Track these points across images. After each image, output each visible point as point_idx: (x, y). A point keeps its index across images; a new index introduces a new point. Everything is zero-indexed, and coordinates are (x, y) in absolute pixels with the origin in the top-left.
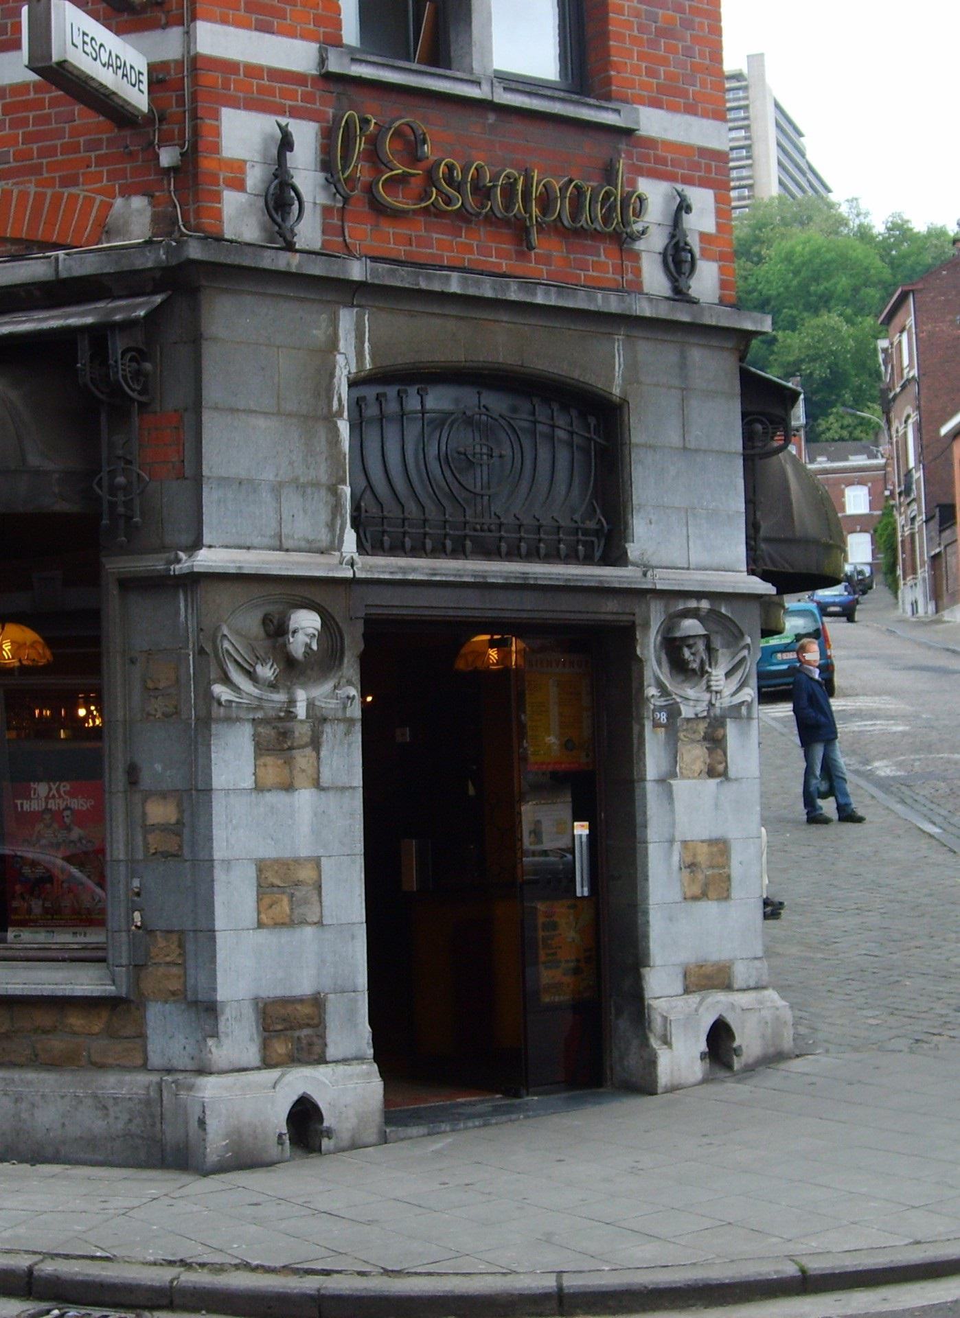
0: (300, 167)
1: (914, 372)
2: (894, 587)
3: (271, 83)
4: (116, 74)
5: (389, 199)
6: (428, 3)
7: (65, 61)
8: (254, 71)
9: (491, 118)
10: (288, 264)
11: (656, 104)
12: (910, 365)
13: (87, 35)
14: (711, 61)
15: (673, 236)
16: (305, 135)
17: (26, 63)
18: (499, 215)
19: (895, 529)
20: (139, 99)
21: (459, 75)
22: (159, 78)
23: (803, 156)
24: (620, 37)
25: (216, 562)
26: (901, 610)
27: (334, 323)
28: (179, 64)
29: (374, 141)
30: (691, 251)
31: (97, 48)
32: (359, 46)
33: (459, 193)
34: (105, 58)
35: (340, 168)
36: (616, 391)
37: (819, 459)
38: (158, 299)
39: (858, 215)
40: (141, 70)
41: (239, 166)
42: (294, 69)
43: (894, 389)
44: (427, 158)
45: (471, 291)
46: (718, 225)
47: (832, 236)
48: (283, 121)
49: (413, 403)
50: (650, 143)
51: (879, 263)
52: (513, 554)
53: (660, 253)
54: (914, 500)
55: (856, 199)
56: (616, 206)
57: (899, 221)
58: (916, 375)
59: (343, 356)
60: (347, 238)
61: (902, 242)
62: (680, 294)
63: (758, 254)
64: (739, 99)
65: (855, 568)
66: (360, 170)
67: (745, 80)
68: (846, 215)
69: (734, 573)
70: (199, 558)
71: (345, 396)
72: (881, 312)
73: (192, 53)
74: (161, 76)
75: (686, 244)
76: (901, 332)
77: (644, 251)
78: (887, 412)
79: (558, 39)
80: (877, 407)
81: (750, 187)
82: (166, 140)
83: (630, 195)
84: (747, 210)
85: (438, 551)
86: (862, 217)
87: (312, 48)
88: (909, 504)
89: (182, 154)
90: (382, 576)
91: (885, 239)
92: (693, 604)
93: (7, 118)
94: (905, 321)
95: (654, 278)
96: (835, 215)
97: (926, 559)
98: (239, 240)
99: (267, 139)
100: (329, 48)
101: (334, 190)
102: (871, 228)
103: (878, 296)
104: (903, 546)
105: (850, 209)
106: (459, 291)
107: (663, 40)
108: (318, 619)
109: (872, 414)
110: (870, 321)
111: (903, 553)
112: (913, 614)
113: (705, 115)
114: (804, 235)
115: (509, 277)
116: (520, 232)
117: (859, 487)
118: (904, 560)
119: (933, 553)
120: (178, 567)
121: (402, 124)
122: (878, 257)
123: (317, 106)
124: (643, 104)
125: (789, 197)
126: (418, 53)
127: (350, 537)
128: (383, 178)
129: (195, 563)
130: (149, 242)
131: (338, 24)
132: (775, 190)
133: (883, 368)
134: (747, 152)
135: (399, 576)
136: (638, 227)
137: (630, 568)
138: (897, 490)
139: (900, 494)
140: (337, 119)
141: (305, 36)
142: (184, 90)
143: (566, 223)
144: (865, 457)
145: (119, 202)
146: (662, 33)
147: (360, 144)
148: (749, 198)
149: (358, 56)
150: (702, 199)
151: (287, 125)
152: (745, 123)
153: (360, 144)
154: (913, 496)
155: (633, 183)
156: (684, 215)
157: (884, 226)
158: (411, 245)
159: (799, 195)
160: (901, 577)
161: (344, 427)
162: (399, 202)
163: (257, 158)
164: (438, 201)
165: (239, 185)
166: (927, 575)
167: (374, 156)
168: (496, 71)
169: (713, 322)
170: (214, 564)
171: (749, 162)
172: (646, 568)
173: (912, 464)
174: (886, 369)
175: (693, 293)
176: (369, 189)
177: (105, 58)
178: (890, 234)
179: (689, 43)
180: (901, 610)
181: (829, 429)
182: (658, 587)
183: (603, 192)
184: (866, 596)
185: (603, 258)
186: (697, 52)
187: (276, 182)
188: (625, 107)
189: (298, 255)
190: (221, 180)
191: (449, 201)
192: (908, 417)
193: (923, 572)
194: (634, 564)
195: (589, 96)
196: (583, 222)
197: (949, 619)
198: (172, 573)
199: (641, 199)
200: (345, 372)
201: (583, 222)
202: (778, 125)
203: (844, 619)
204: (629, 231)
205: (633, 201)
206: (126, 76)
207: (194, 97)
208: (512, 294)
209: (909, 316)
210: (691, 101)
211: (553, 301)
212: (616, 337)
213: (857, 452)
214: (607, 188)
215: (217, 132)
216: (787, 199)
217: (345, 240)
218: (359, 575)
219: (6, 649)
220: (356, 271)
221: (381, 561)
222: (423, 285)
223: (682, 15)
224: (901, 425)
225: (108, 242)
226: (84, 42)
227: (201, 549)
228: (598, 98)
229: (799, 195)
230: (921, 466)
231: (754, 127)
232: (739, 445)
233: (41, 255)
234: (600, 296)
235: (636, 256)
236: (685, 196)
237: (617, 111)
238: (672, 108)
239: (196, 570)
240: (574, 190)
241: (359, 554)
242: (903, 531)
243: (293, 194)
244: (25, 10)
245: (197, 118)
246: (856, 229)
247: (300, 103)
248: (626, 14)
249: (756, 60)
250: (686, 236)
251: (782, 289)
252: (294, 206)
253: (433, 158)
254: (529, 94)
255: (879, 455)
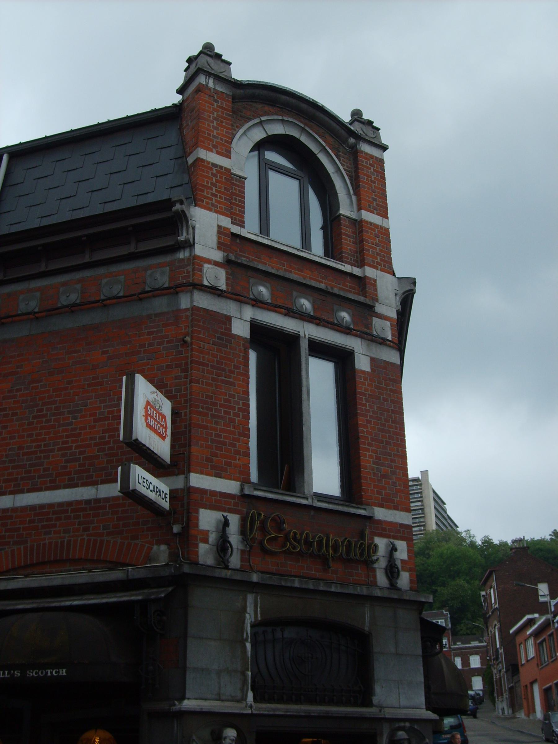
0: (232, 533)
1: (497, 606)
2: (494, 702)
3: (220, 499)
4: (156, 495)
5: (268, 547)
6: (286, 465)
7: (135, 490)
8: (214, 493)
9: (312, 513)
10: (226, 575)
11: (381, 506)
12: (495, 603)
13: (145, 479)
14: (404, 488)
15: (389, 561)
16: (234, 520)
17: (119, 490)
18: (316, 553)
19: (492, 675)
20: (165, 504)
21: (299, 495)
22: (174, 495)
23: (446, 512)
24: (366, 467)
25: (191, 706)
26: (497, 713)
27: (245, 600)
28: (182, 490)
29: (263, 523)
30: (397, 568)
31: (149, 484)
32: (257, 483)
33: (299, 544)
34: (152, 488)
35: (248, 534)
36: (367, 629)
37: (458, 643)
38: (170, 589)
39: (470, 537)
40: (167, 493)
41: (206, 533)
42: (230, 492)
43: (489, 613)
44: (285, 530)
45: (304, 586)
46: (409, 556)
47: (459, 547)
48: (225, 514)
49: (279, 635)
50: (379, 522)
51: (479, 557)
52: (322, 702)
53: (384, 569)
54: (500, 662)
55: (469, 530)
56: (365, 549)
57: (487, 540)
58: (498, 607)
59: (248, 614)
60: (251, 564)
61: (489, 549)
62: (393, 586)
63: (428, 554)
64: (418, 489)
65: (476, 692)
66: (257, 534)
67: (420, 481)
68: (465, 537)
69: (420, 710)
70: (184, 704)
71: (249, 632)
72: (482, 579)
73: (188, 486)
74: (175, 495)
75: (395, 565)
76: (491, 588)
77: (377, 568)
78: (486, 623)
79: (340, 479)
80: (482, 620)
81: (424, 526)
82: (176, 522)
83: (371, 544)
84: (423, 536)
85: (289, 701)
86: (471, 538)
87: (238, 484)
88: (498, 664)
89: (182, 528)
90: (264, 713)
91: (482, 547)
92: (402, 724)
93: (110, 510)
94: (492, 583)
95: (382, 579)
96: (460, 537)
97: (507, 688)
98: (205, 564)
99: (218, 521)
100: (245, 484)
101: (246, 543)
102: (475, 542)
103: (480, 572)
104: (496, 684)
105: (466, 535)
106: (298, 586)
107: (383, 480)
108: (235, 732)
109: (479, 623)
110: (477, 582)
111: (497, 686)
112: (502, 714)
113: (402, 510)
114: (447, 546)
115: (320, 580)
116: (325, 561)
117: (476, 656)
118: (497, 689)
119: (510, 686)
120: (174, 708)
121: (274, 516)
122: (479, 555)
123: (240, 508)
124: (375, 506)
125: (440, 530)
126: (282, 485)
127: (250, 695)
128: (267, 538)
129: (182, 706)
130: (167, 565)
131: (249, 474)
132: (434, 527)
133: (483, 604)
134: (422, 511)
135: (271, 713)
136: (375, 558)
137: (374, 708)
138: (492, 658)
139: (494, 660)
140: (248, 513)
141: (235, 479)
142: (184, 501)
143: (344, 557)
144: (477, 642)
145: (155, 547)
146: (383, 476)
147: (257, 524)
148: (423, 530)
149: (257, 487)
150: (401, 545)
151: (227, 516)
152: (421, 499)
153: (257, 524)
154: (499, 660)
155: (373, 540)
156: (394, 553)
157: (481, 542)
158: (278, 566)
159: (445, 529)
160: (496, 698)
161: (248, 645)
162: (274, 548)
163: (214, 529)
164: (290, 548)
165: (206, 541)
166: (507, 696)
167: (263, 529)
168: (314, 492)
169: (407, 598)
170: (190, 707)
171: (423, 515)
172: (381, 708)
173: (498, 646)
174: (485, 604)
175: (399, 585)
176: (261, 543)
177: (152, 488)
178: (483, 545)
179: (394, 481)
180: (497, 713)
181: (461, 630)
182: (387, 716)
183: (360, 543)
184: (481, 705)
185: (360, 571)
186: (398, 484)
187: (222, 540)
188: (368, 508)
189: (230, 571)
190: (199, 539)
191: (294, 548)
192: (496, 625)
193: (506, 695)
194: (376, 706)
195: (353, 504)
196: (351, 556)
197: (519, 717)
198: (171, 710)
199: (376, 546)
200: (249, 621)
201: (351, 556)
202: (435, 500)
203: (472, 717)
204: (371, 559)
205: (372, 547)
206: (160, 495)
207: (188, 504)
208: (321, 587)
209: (494, 581)
210: (396, 504)
211: (339, 590)
212: (366, 605)
213: (474, 640)
214: (361, 541)
215: (197, 519)
216: (439, 531)
217: (250, 565)
218: (254, 712)
219: (97, 741)
220: (255, 578)
221: (264, 705)
222: (283, 583)
223: (391, 469)
224: (492, 629)
225: (150, 564)
226: (144, 482)
227: (185, 700)
228: (357, 504)
229: (445, 529)
230: (502, 647)
231: (425, 501)
232: (420, 652)
233: (121, 569)
234: (359, 588)
235: (374, 570)
236: (394, 544)
237: (365, 509)
238: (388, 508)
239: (182, 709)
240: (348, 543)
241: (255, 703)
242: (496, 676)
243: (228, 545)
244: (120, 468)
245: (189, 513)
246: (469, 543)
247: (232, 507)
248: (368, 469)
249: (425, 473)
250: (395, 561)
251: (439, 569)
252: (229, 550)
253: (288, 530)
254: (328, 503)
255: (484, 641)
